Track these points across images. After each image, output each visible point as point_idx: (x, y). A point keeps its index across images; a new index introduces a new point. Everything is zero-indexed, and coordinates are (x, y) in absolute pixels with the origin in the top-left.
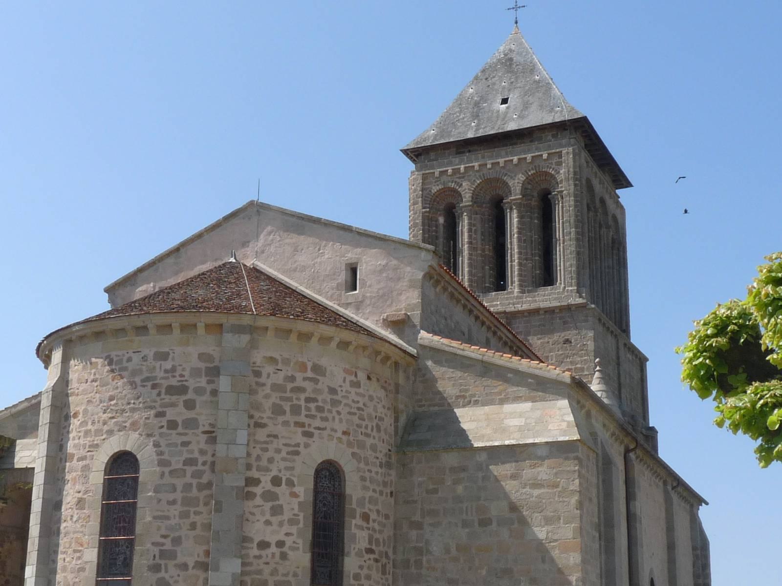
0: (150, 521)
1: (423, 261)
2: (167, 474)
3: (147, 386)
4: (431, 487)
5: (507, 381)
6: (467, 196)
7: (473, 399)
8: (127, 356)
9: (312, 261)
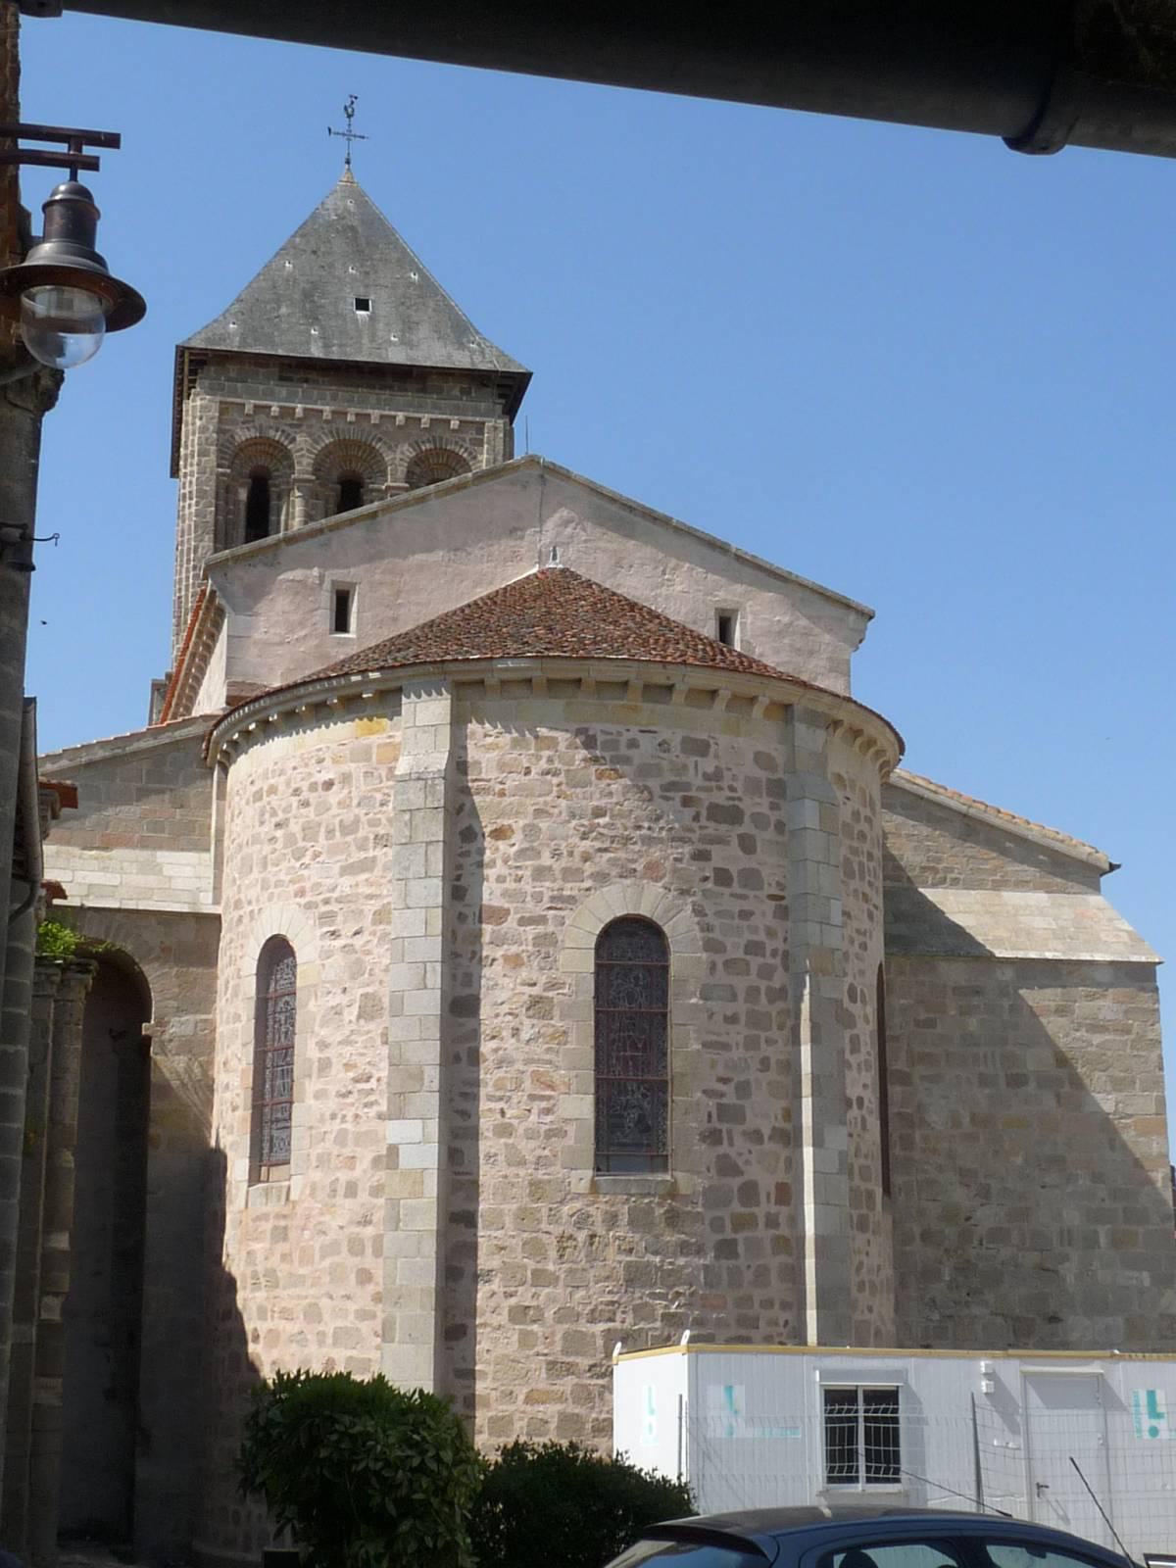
0: (698, 1050)
1: (852, 630)
2: (720, 967)
3: (673, 799)
4: (923, 1016)
5: (1004, 852)
6: (304, 463)
7: (950, 876)
8: (627, 736)
9: (652, 590)
